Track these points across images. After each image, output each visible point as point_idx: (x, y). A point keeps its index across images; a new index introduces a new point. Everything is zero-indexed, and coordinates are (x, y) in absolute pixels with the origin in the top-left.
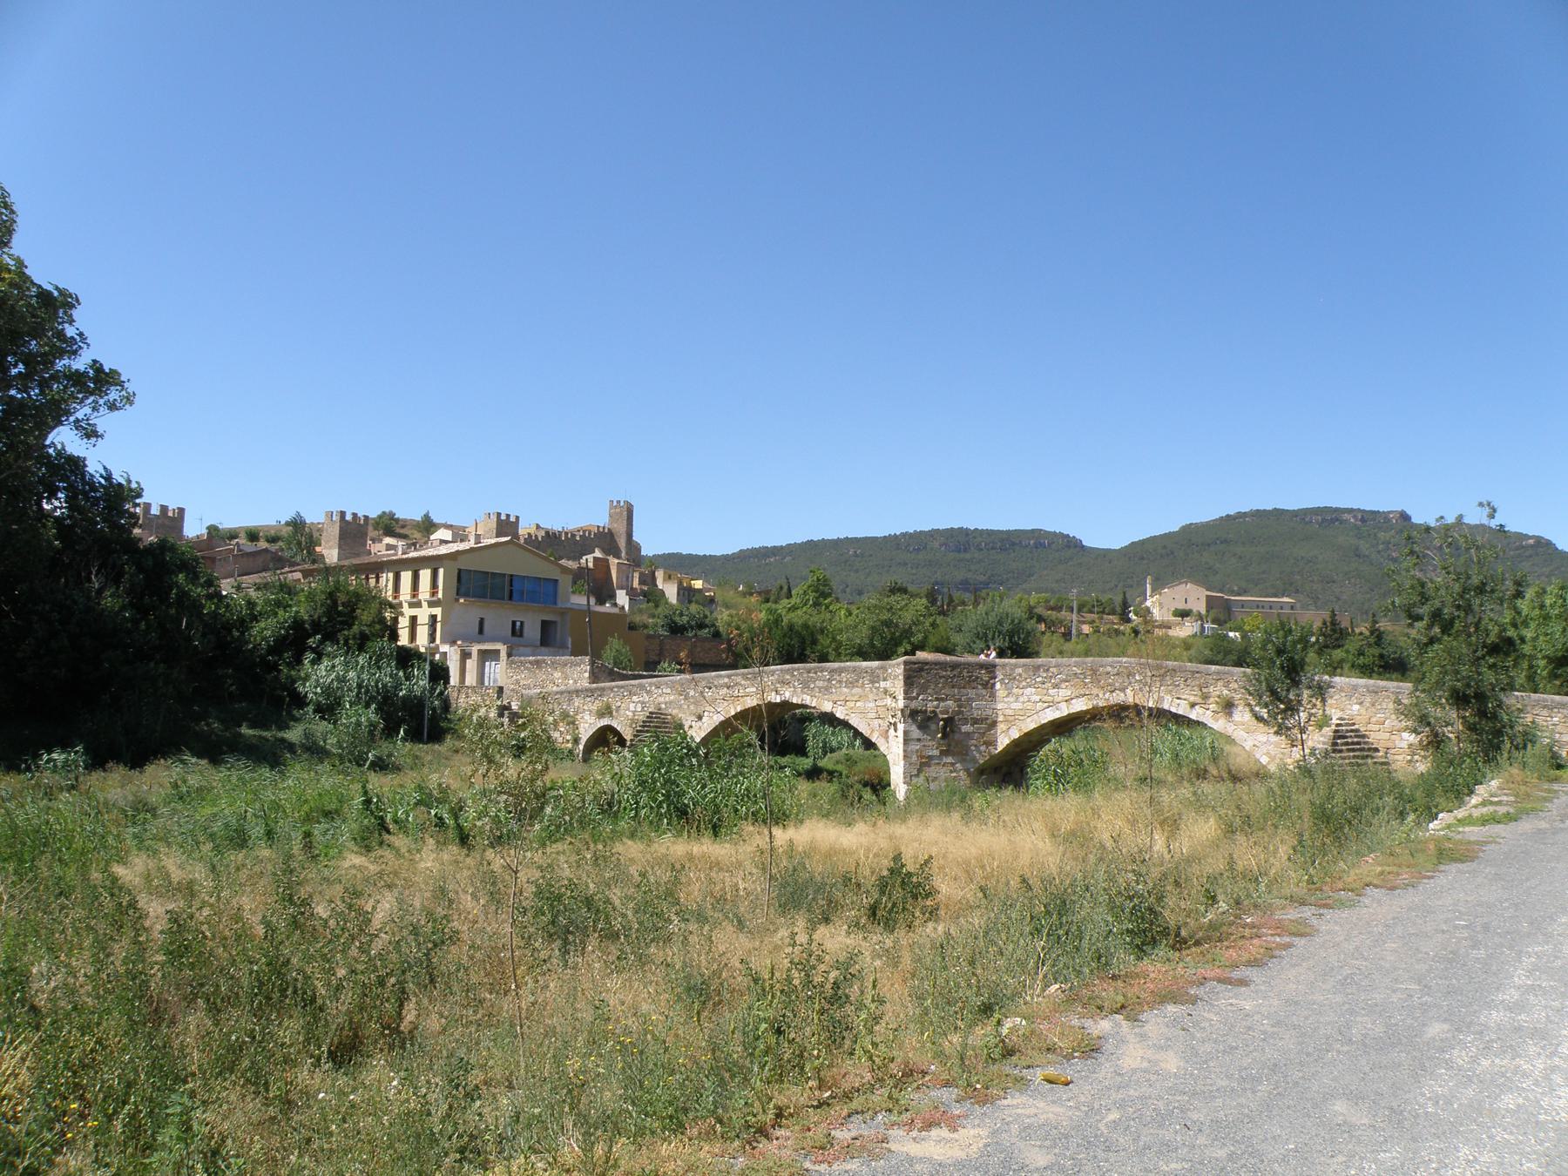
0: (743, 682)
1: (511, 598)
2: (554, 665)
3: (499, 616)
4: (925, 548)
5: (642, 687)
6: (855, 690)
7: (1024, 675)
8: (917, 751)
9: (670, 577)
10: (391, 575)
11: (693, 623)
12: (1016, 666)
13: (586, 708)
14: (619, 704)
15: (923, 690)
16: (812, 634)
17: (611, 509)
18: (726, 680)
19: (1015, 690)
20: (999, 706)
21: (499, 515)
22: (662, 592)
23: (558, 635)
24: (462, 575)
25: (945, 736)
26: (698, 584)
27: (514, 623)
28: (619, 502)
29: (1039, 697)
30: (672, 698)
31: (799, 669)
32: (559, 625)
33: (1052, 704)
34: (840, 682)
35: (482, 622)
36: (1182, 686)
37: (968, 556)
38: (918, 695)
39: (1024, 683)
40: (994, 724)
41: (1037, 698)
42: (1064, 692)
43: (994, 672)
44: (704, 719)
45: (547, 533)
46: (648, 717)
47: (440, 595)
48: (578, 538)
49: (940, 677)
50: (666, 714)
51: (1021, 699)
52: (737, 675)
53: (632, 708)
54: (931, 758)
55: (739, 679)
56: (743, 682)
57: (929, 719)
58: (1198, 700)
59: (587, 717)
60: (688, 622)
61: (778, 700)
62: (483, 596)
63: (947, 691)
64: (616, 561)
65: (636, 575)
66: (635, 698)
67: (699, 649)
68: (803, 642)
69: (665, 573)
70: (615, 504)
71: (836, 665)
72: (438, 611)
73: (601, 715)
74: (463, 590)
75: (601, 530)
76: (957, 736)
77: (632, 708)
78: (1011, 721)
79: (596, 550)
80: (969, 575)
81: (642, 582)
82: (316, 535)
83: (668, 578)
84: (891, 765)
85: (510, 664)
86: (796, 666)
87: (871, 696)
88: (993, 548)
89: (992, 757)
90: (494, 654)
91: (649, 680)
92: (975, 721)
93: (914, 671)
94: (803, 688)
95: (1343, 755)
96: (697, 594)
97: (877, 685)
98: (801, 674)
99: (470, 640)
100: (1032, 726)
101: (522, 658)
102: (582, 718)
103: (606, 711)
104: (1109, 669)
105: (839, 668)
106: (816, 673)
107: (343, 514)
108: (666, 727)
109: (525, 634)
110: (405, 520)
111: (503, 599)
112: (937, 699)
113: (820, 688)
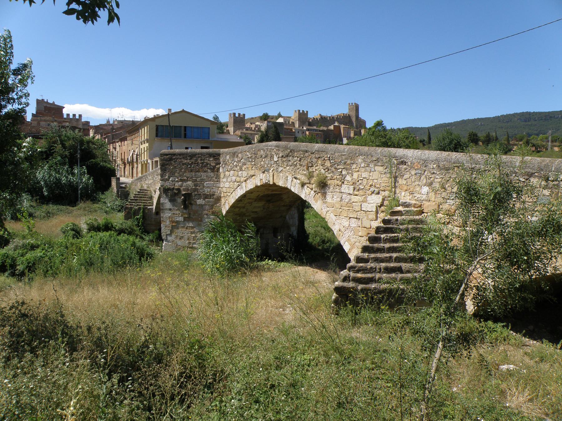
1: (185, 137)
4: (511, 121)
8: (169, 217)
15: (172, 174)
21: (299, 111)
28: (352, 104)
36: (298, 166)
37: (530, 123)
38: (169, 177)
43: (219, 159)
49: (183, 164)
54: (178, 222)
57: (176, 194)
58: (306, 181)
63: (187, 174)
74: (159, 134)
76: (194, 207)
88: (541, 120)
92: (206, 197)
108: (145, 197)
111: (181, 137)
112: (181, 180)
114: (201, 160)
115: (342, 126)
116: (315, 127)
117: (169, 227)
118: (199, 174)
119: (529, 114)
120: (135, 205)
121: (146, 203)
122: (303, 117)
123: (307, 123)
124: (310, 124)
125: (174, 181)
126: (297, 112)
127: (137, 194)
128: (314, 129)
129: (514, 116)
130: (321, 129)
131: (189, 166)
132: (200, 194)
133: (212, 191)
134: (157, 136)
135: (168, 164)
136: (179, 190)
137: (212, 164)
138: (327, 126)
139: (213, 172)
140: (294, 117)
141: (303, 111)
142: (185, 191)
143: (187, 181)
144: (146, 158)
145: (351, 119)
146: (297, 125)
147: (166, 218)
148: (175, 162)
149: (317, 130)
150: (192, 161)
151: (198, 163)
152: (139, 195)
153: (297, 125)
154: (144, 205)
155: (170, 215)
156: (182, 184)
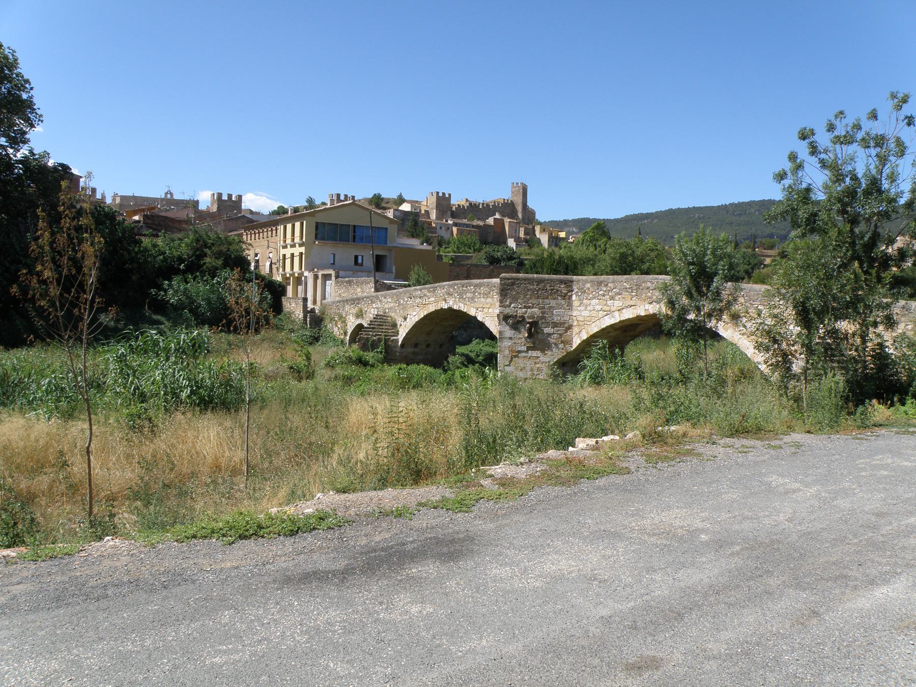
0: (428, 294)
1: (354, 241)
3: (345, 253)
6: (489, 300)
7: (591, 289)
9: (544, 231)
10: (282, 226)
11: (505, 256)
12: (586, 282)
15: (515, 299)
17: (512, 188)
18: (419, 292)
19: (585, 301)
21: (438, 193)
23: (388, 264)
25: (531, 335)
26: (562, 235)
27: (356, 257)
28: (517, 183)
29: (601, 307)
30: (392, 305)
33: (609, 313)
34: (480, 294)
35: (356, 257)
38: (511, 303)
39: (591, 296)
40: (570, 327)
41: (598, 307)
42: (618, 303)
43: (571, 286)
45: (470, 204)
47: (304, 240)
49: (528, 290)
50: (387, 317)
51: (589, 308)
52: (425, 289)
54: (519, 352)
55: (425, 292)
56: (428, 294)
57: (519, 322)
59: (351, 318)
60: (502, 256)
61: (446, 307)
64: (509, 220)
69: (541, 228)
70: (515, 185)
71: (478, 281)
72: (303, 249)
74: (320, 236)
75: (506, 201)
76: (540, 336)
78: (583, 324)
85: (337, 282)
86: (457, 282)
89: (569, 353)
92: (555, 325)
93: (508, 285)
94: (460, 298)
95: (206, 454)
100: (596, 330)
104: (649, 284)
105: (480, 283)
106: (466, 287)
109: (364, 264)
110: (389, 199)
111: (349, 241)
112: (525, 307)
113: (469, 298)
114: (551, 286)
115: (507, 220)
116: (465, 221)
117: (508, 357)
118: (547, 301)
120: (372, 335)
121: (388, 333)
122: (443, 202)
123: (449, 213)
124: (454, 215)
125: (517, 307)
126: (435, 195)
127: (373, 321)
128: (465, 224)
129: (750, 205)
130: (475, 224)
133: (562, 319)
134: (316, 238)
135: (509, 289)
136: (523, 317)
137: (563, 291)
139: (564, 299)
141: (444, 194)
143: (533, 308)
144: (296, 269)
146: (433, 216)
147: (505, 347)
148: (518, 287)
149: (470, 225)
150: (539, 287)
152: (375, 321)
153: (433, 216)
154: (386, 336)
156: (526, 311)
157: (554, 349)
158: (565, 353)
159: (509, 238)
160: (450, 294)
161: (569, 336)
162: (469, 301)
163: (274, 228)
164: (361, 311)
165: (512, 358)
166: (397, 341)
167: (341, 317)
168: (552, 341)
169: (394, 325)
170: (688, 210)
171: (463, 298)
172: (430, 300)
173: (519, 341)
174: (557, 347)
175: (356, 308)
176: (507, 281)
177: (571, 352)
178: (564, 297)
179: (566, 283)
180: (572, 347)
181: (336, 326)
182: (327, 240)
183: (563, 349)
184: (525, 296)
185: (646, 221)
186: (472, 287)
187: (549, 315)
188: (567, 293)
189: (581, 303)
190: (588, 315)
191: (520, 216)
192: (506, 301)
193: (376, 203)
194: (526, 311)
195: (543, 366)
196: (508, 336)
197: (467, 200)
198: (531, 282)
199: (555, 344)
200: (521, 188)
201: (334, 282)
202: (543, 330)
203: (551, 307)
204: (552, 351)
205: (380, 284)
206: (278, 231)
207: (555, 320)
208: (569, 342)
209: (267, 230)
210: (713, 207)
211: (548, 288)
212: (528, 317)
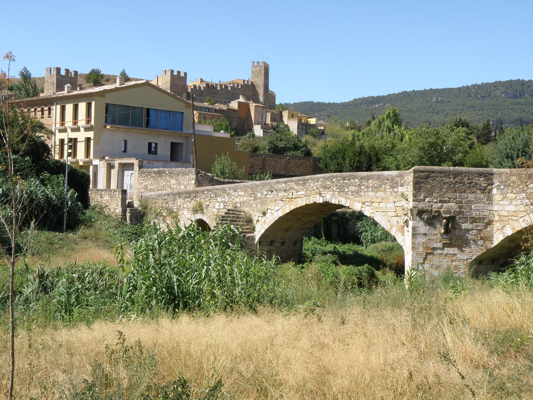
1: (147, 127)
2: (171, 175)
4: (489, 95)
5: (224, 190)
6: (380, 194)
8: (423, 244)
9: (293, 116)
10: (59, 107)
13: (185, 206)
14: (208, 203)
15: (430, 193)
16: (376, 155)
17: (253, 67)
18: (284, 185)
19: (509, 195)
20: (496, 208)
21: (172, 71)
22: (287, 126)
23: (184, 153)
24: (109, 107)
26: (313, 121)
27: (150, 144)
31: (337, 177)
32: (184, 145)
34: (368, 187)
37: (523, 101)
38: (425, 197)
40: (490, 223)
43: (491, 179)
44: (268, 215)
45: (207, 85)
46: (226, 213)
47: (93, 123)
48: (230, 89)
50: (240, 211)
52: (291, 181)
53: (217, 207)
54: (435, 249)
55: (293, 185)
56: (296, 187)
57: (434, 217)
59: (186, 212)
61: (321, 202)
62: (126, 124)
63: (450, 195)
64: (255, 104)
65: (269, 115)
66: (219, 199)
67: (292, 165)
68: (370, 160)
69: (289, 113)
70: (256, 64)
72: (91, 134)
73: (195, 211)
74: (109, 120)
75: (246, 83)
76: (457, 232)
77: (217, 207)
78: (505, 220)
79: (241, 97)
80: (523, 115)
81: (272, 120)
82: (38, 83)
83: (292, 116)
84: (405, 254)
85: (141, 174)
87: (391, 199)
89: (488, 250)
90: (130, 166)
91: (229, 185)
92: (474, 220)
93: (422, 178)
96: (312, 128)
97: (396, 190)
98: (338, 181)
99: (114, 156)
101: (149, 169)
102: (183, 214)
103: (199, 209)
105: (367, 176)
106: (349, 180)
107: (58, 70)
109: (159, 152)
110: (109, 76)
111: (142, 126)
112: (441, 201)
113: (352, 192)
114: (469, 179)
116: (206, 104)
118: (465, 195)
119: (521, 83)
125: (432, 202)
126: (169, 74)
128: (206, 108)
129: (495, 87)
130: (217, 108)
131: (452, 186)
132: (467, 218)
133: (482, 214)
135: (424, 182)
137: (483, 185)
138: (227, 103)
139: (483, 193)
140: (164, 83)
141: (179, 72)
142: (446, 214)
143: (449, 202)
145: (256, 91)
149: (212, 109)
150: (457, 180)
151: (464, 183)
155: (424, 240)
156: (442, 206)
157: (472, 246)
158: (485, 250)
159: (256, 124)
160: (325, 187)
161: (489, 232)
162: (352, 195)
163: (46, 108)
164: (200, 205)
165: (426, 255)
166: (253, 238)
167: (170, 212)
168: (470, 237)
169: (250, 221)
170: (424, 93)
171: (344, 191)
172: (298, 193)
173: (435, 238)
174: (476, 244)
175: (193, 201)
176: (421, 174)
177: (491, 249)
178: (483, 190)
179: (486, 176)
180: (492, 243)
181: (164, 221)
182: (118, 124)
183: (482, 246)
184: (441, 189)
185: (377, 106)
186: (357, 180)
187: (467, 209)
188: (487, 187)
189: (504, 198)
190: (514, 210)
191: (261, 99)
192: (420, 195)
193: (95, 80)
194: (442, 206)
195: (461, 263)
196: (423, 232)
197: (202, 81)
198: (447, 174)
199: (474, 241)
200: (263, 68)
201: (137, 173)
202: (460, 226)
203: (469, 201)
204: (470, 247)
205: (201, 176)
206: (53, 112)
207: (474, 215)
208: (488, 238)
209: (35, 110)
210: (453, 89)
211: (466, 181)
212: (444, 212)
